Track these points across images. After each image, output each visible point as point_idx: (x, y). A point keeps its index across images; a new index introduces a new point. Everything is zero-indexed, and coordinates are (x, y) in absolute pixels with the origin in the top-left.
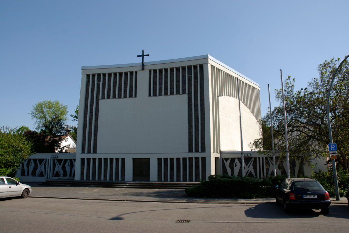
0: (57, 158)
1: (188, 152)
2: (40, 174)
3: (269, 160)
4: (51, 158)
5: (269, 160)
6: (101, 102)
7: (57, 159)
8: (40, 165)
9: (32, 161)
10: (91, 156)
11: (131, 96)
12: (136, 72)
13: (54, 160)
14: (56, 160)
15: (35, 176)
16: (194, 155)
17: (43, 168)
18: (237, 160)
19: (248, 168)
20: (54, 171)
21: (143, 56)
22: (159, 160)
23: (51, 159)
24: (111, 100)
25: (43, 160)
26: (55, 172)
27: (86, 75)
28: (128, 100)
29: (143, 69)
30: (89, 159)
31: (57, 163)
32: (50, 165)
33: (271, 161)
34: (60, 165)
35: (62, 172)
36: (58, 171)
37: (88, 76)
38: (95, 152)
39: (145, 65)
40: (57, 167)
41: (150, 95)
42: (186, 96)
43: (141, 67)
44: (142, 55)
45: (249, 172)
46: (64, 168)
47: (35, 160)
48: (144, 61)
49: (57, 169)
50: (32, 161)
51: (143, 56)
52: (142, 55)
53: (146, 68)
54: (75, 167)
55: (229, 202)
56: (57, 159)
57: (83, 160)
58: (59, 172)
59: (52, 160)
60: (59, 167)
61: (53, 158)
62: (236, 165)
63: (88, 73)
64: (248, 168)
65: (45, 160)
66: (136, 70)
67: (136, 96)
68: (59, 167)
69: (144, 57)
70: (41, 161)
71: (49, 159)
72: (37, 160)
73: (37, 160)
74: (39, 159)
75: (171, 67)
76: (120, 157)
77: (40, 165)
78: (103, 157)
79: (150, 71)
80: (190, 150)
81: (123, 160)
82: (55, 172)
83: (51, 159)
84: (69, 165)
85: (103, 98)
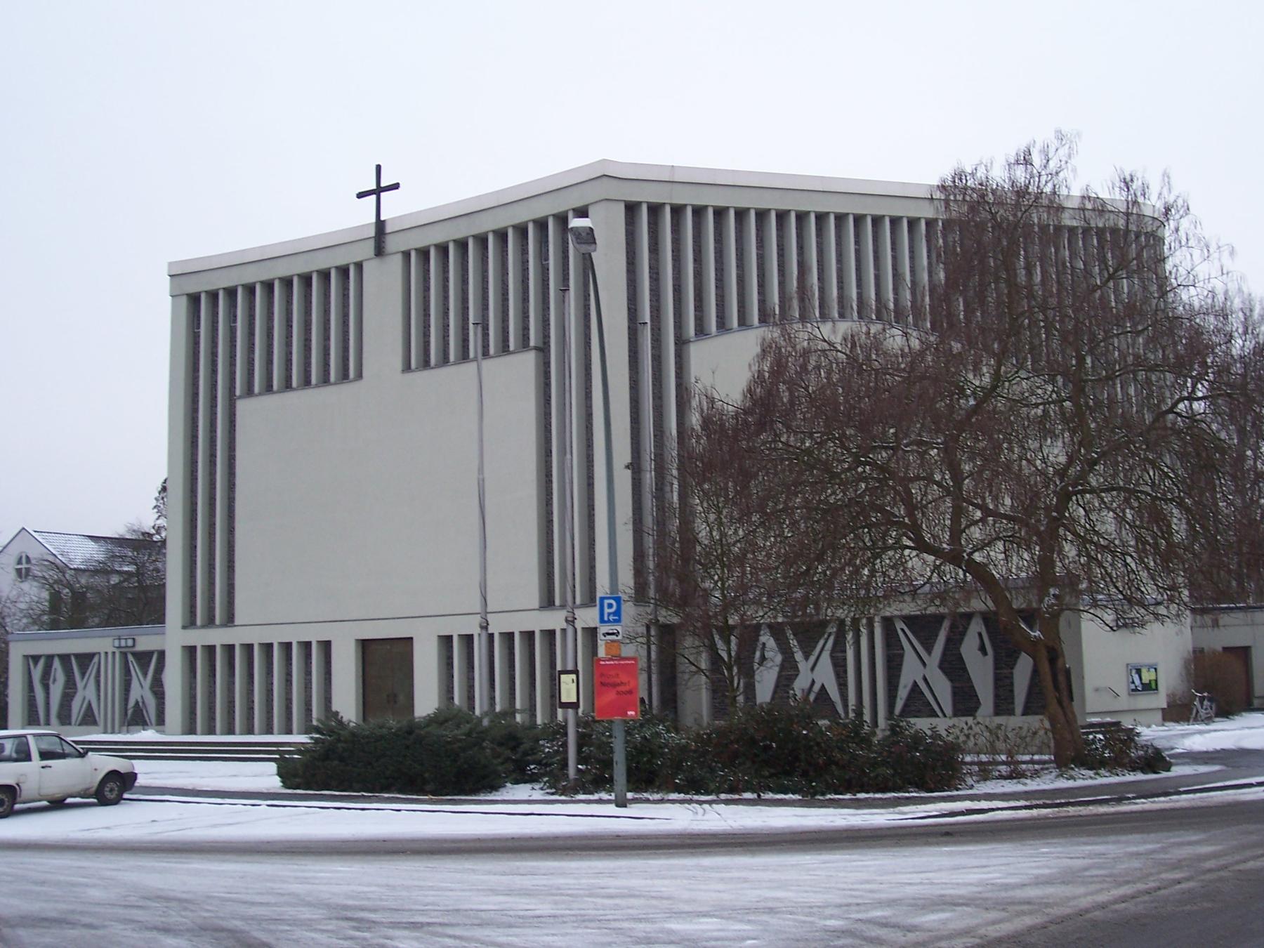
0: (134, 646)
1: (536, 605)
2: (86, 715)
3: (902, 630)
4: (110, 650)
5: (902, 630)
6: (242, 406)
7: (134, 654)
8: (83, 678)
9: (57, 664)
10: (217, 637)
11: (344, 376)
12: (359, 266)
13: (124, 655)
14: (130, 658)
15: (70, 724)
16: (555, 620)
17: (90, 693)
18: (981, 622)
19: (813, 669)
20: (126, 699)
21: (378, 191)
22: (446, 641)
23: (114, 653)
24: (492, 360)
25: (90, 656)
26: (131, 703)
27: (184, 300)
28: (346, 390)
29: (380, 251)
30: (210, 650)
31: (908, 642)
32: (112, 674)
33: (134, 667)
34: (145, 674)
35: (943, 689)
36: (140, 700)
37: (194, 299)
38: (230, 620)
39: (389, 229)
40: (910, 659)
41: (407, 368)
42: (528, 361)
43: (372, 244)
44: (374, 187)
45: (816, 688)
46: (953, 666)
47: (65, 658)
48: (382, 218)
49: (911, 672)
50: (57, 664)
51: (378, 191)
52: (374, 187)
53: (392, 244)
54: (1064, 657)
55: (1194, 838)
56: (134, 654)
57: (190, 651)
58: (143, 702)
59: (117, 655)
60: (924, 664)
61: (120, 647)
62: (55, 680)
63: (193, 289)
64: (813, 669)
65: (96, 659)
66: (358, 259)
67: (360, 375)
68: (924, 664)
69: (383, 194)
70: (85, 660)
71: (106, 653)
72: (73, 659)
73: (73, 659)
74: (77, 656)
75: (516, 221)
76: (314, 635)
77: (83, 678)
78: (256, 637)
79: (406, 255)
80: (548, 602)
81: (326, 646)
82: (131, 703)
83: (114, 653)
84: (983, 649)
85: (249, 392)
